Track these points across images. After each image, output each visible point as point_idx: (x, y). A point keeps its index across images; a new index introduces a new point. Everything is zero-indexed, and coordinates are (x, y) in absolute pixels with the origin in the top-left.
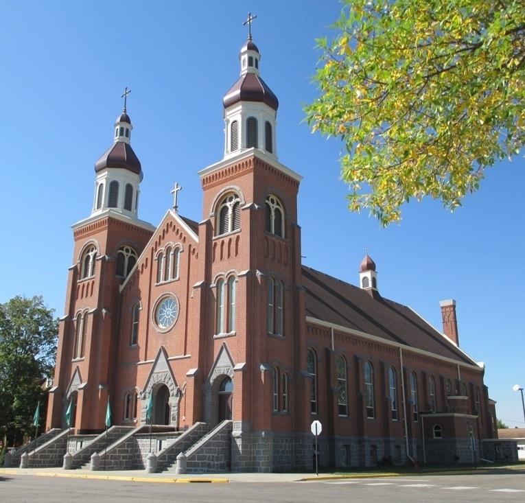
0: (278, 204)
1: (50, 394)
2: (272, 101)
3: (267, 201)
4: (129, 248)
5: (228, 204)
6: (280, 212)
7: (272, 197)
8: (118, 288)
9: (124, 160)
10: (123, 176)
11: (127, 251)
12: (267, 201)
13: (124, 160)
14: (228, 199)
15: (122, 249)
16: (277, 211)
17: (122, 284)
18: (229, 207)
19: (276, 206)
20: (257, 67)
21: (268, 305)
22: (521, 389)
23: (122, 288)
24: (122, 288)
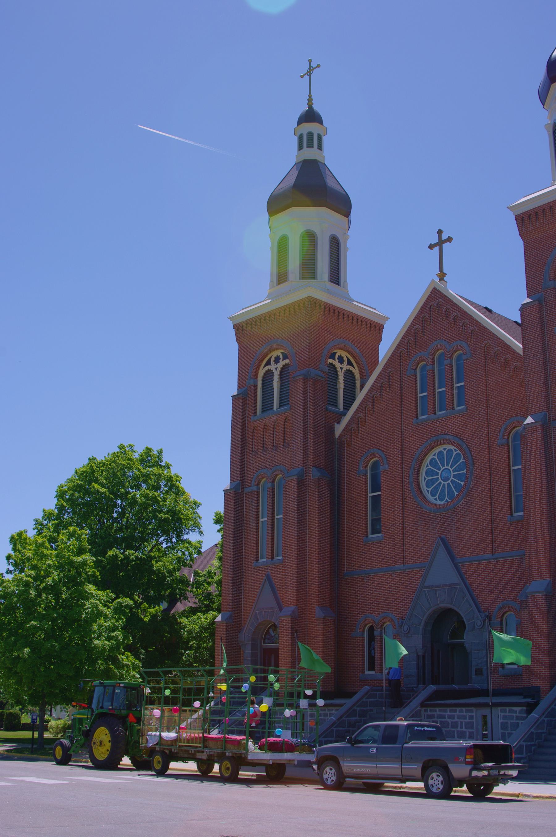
0: (349, 363)
1: (31, 732)
2: (341, 204)
3: (330, 361)
4: (344, 354)
5: (272, 367)
6: (353, 374)
7: (340, 353)
8: (331, 430)
9: (312, 186)
10: (317, 218)
11: (341, 360)
12: (330, 361)
13: (312, 186)
14: (273, 359)
15: (333, 356)
16: (349, 375)
17: (339, 423)
18: (274, 371)
19: (345, 367)
20: (320, 147)
21: (466, 482)
22: (108, 750)
23: (339, 429)
24: (339, 429)
